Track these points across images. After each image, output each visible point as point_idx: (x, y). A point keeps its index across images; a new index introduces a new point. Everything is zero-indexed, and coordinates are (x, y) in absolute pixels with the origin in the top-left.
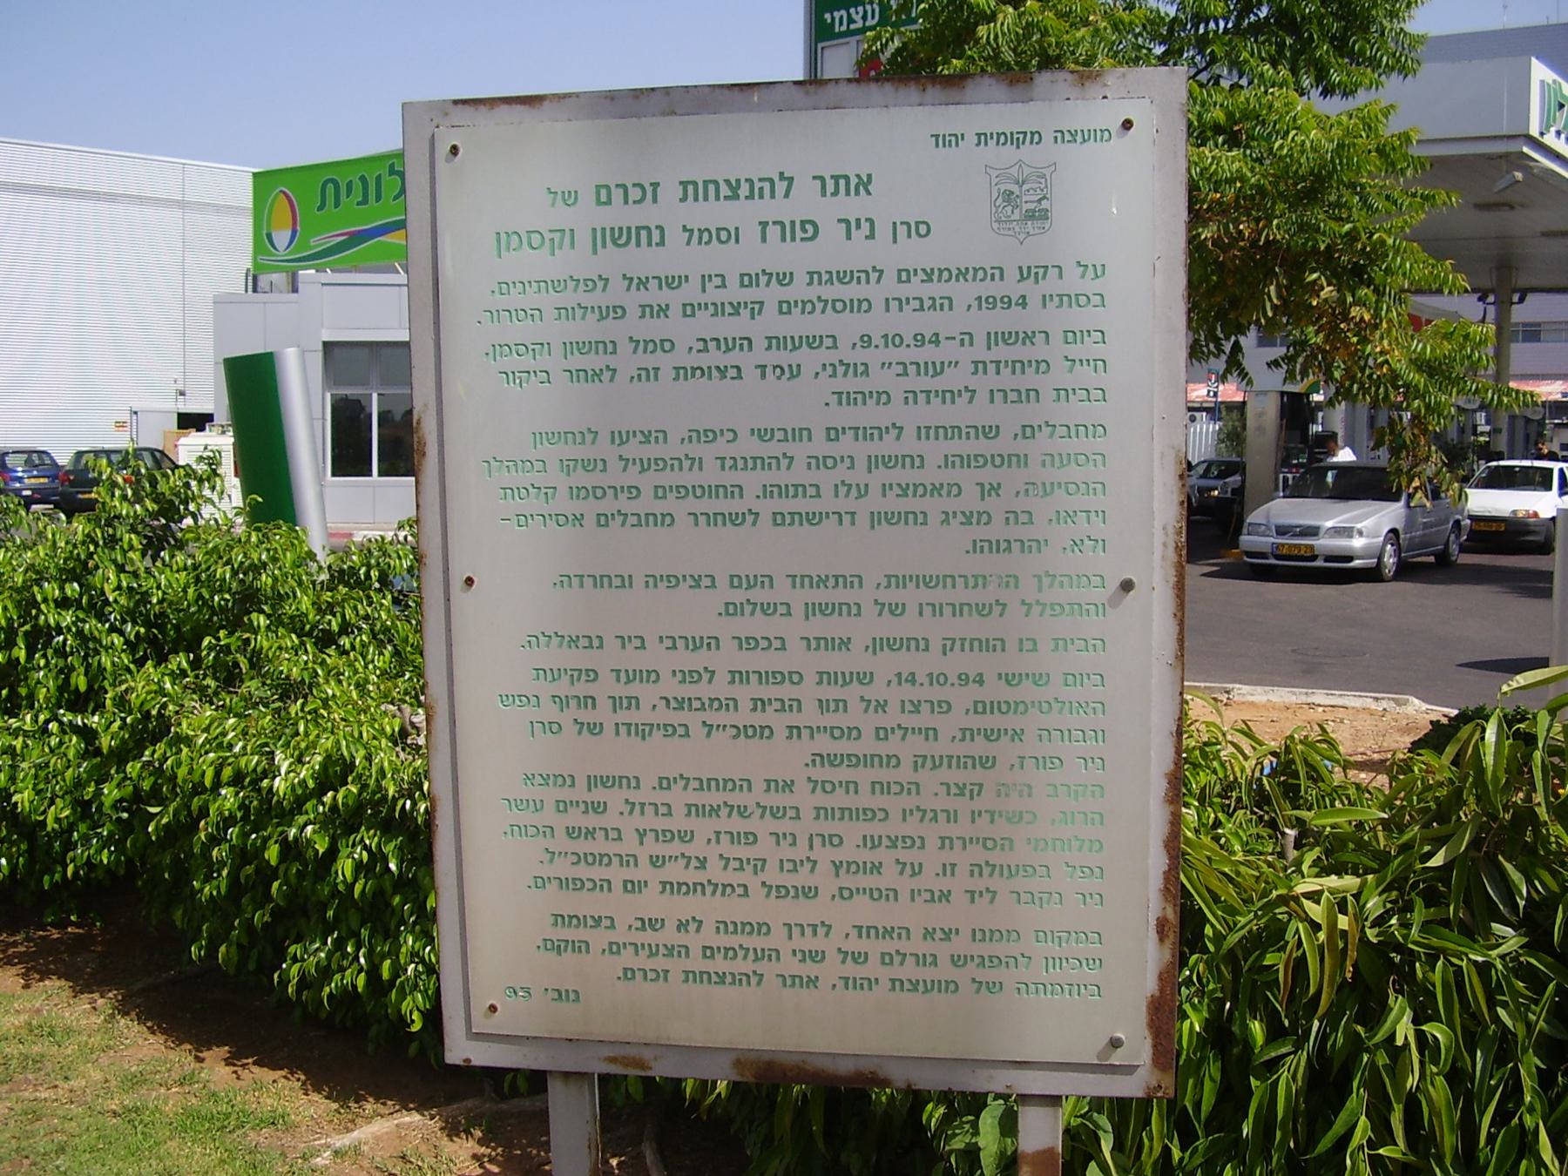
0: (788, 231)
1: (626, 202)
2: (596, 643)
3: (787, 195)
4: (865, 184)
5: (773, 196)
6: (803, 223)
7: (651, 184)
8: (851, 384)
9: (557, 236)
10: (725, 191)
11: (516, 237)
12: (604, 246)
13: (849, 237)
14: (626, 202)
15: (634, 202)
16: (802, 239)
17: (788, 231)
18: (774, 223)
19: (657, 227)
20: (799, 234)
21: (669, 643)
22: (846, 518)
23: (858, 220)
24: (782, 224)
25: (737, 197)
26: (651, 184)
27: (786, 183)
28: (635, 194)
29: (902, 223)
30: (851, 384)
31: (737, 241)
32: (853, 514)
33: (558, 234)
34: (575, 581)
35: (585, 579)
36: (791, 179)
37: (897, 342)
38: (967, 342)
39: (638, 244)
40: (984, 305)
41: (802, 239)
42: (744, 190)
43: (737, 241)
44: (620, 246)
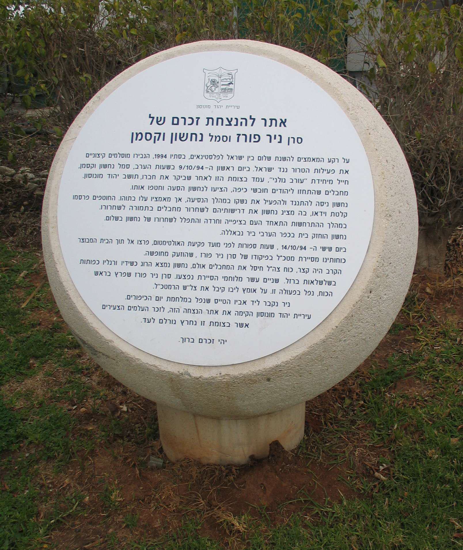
0: (248, 138)
1: (185, 124)
2: (241, 233)
3: (252, 125)
4: (283, 123)
5: (246, 125)
6: (255, 135)
7: (270, 119)
8: (88, 171)
9: (157, 135)
10: (226, 122)
11: (218, 137)
12: (176, 140)
13: (270, 142)
14: (185, 124)
15: (189, 124)
16: (254, 142)
17: (248, 138)
18: (243, 135)
19: (279, 135)
20: (253, 140)
21: (262, 234)
22: (242, 211)
23: (275, 136)
24: (245, 135)
25: (230, 125)
26: (197, 118)
27: (152, 119)
28: (189, 121)
29: (292, 138)
30: (88, 171)
31: (230, 141)
32: (244, 210)
33: (159, 135)
34: (209, 221)
35: (212, 220)
36: (254, 119)
37: (190, 168)
38: (211, 169)
39: (191, 140)
40: (157, 157)
41: (254, 142)
42: (234, 122)
43: (230, 141)
44: (181, 140)
